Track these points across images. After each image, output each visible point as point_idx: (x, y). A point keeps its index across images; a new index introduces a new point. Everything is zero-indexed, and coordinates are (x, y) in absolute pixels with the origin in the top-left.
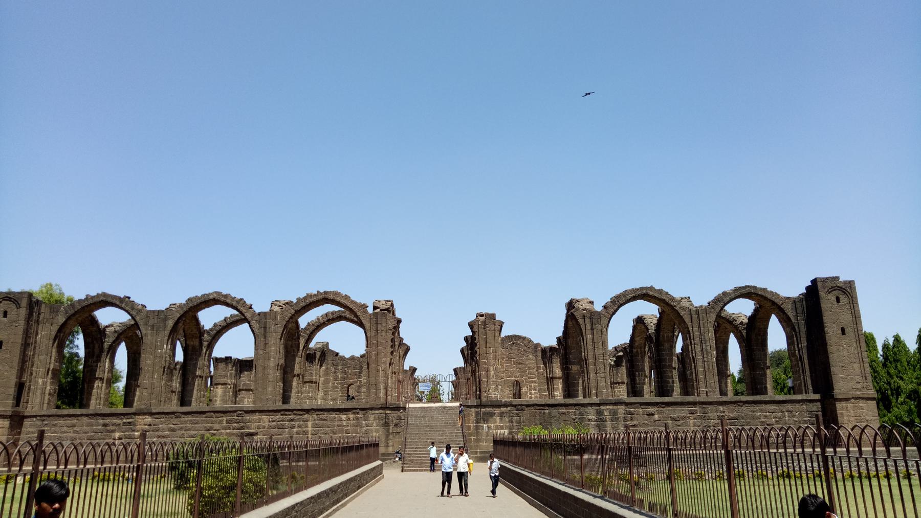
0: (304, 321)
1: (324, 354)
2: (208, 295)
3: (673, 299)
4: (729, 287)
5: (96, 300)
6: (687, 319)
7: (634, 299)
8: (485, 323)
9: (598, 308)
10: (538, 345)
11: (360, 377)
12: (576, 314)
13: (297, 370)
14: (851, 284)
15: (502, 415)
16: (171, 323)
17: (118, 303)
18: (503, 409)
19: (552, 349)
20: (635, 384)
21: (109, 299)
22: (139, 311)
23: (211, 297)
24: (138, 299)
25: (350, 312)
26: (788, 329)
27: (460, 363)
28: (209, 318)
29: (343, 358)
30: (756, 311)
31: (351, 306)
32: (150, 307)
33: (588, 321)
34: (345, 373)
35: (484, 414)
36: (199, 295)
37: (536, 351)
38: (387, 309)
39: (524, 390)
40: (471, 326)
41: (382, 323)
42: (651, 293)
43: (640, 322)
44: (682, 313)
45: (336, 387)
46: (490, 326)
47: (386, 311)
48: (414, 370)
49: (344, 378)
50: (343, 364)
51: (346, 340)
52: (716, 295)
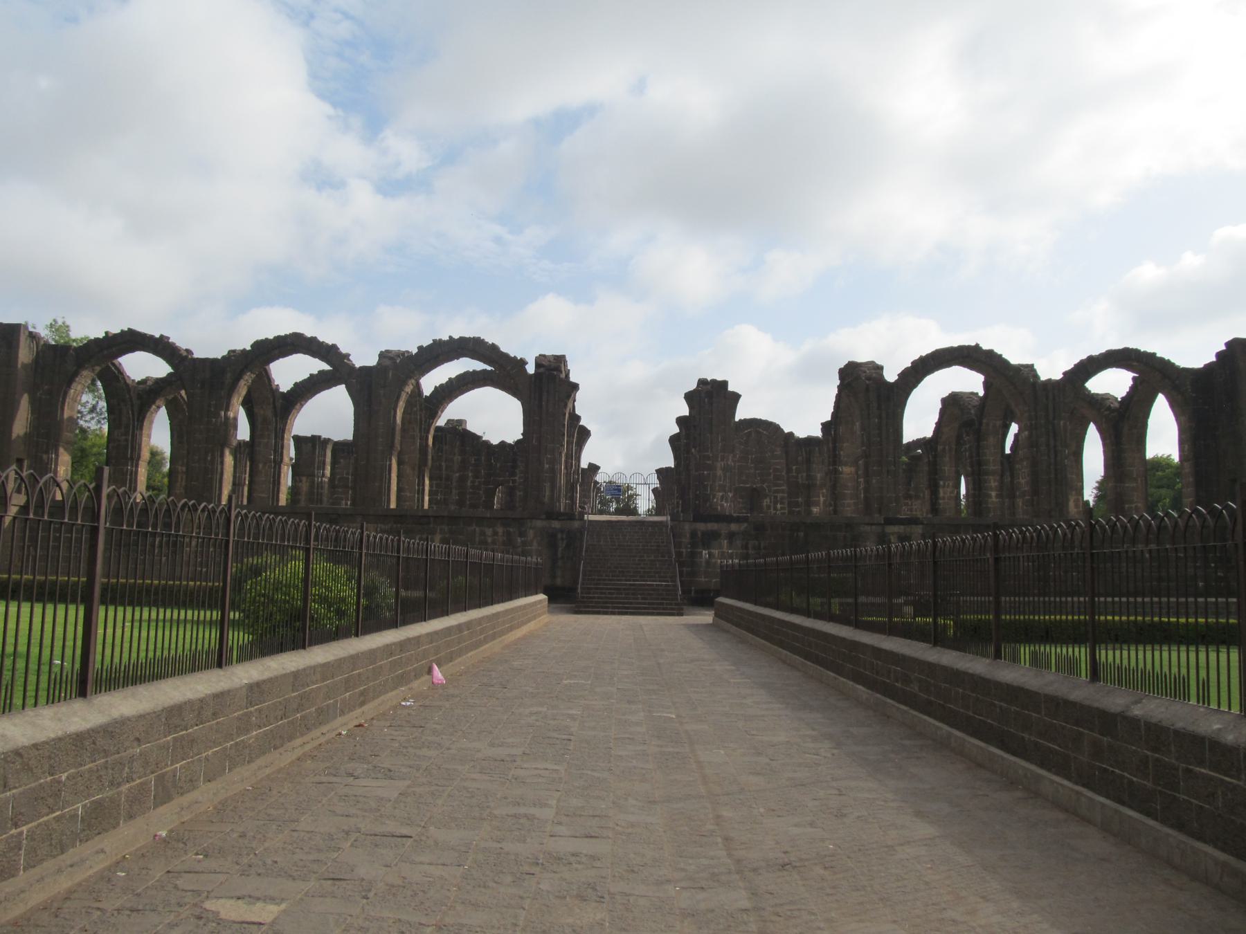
0: (430, 382)
1: (457, 431)
4: (1097, 349)
11: (513, 474)
13: (166, 480)
15: (731, 536)
18: (734, 527)
19: (810, 441)
20: (937, 498)
24: (181, 340)
26: (1182, 418)
30: (1133, 389)
32: (198, 354)
35: (703, 534)
36: (271, 337)
40: (689, 397)
41: (546, 390)
43: (953, 404)
48: (594, 468)
51: (495, 417)
52: (1077, 361)
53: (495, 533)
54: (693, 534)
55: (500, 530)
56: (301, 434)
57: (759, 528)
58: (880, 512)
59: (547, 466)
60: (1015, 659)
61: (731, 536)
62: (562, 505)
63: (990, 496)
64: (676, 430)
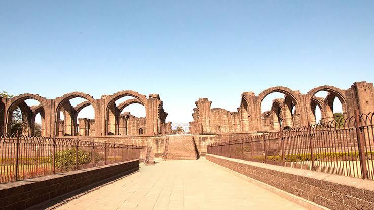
4: (317, 86)
11: (145, 125)
18: (212, 136)
24: (42, 96)
53: (139, 141)
54: (200, 138)
55: (140, 140)
57: (220, 136)
60: (289, 166)
61: (211, 138)
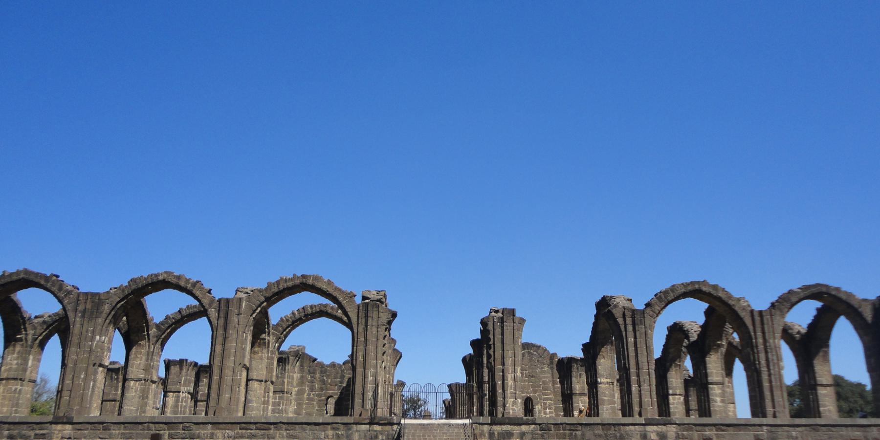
0: (278, 312)
2: (157, 275)
3: (730, 297)
4: (795, 286)
5: (15, 278)
6: (748, 321)
7: (684, 295)
8: (502, 320)
9: (639, 305)
10: (554, 355)
12: (614, 311)
14: (583, 345)
16: (106, 308)
17: (42, 282)
18: (524, 428)
21: (32, 278)
22: (69, 293)
23: (160, 278)
24: (69, 279)
25: (337, 307)
27: (461, 377)
28: (160, 306)
29: (322, 365)
31: (335, 294)
33: (629, 320)
34: (323, 382)
36: (145, 276)
37: (552, 363)
38: (379, 300)
39: (537, 408)
42: (704, 289)
43: (676, 331)
44: (742, 314)
45: (312, 400)
46: (508, 326)
47: (372, 305)
49: (322, 389)
50: (321, 372)
52: (779, 294)
55: (330, 433)
56: (172, 358)
58: (640, 415)
59: (370, 378)
62: (382, 412)
63: (716, 401)
64: (470, 351)
